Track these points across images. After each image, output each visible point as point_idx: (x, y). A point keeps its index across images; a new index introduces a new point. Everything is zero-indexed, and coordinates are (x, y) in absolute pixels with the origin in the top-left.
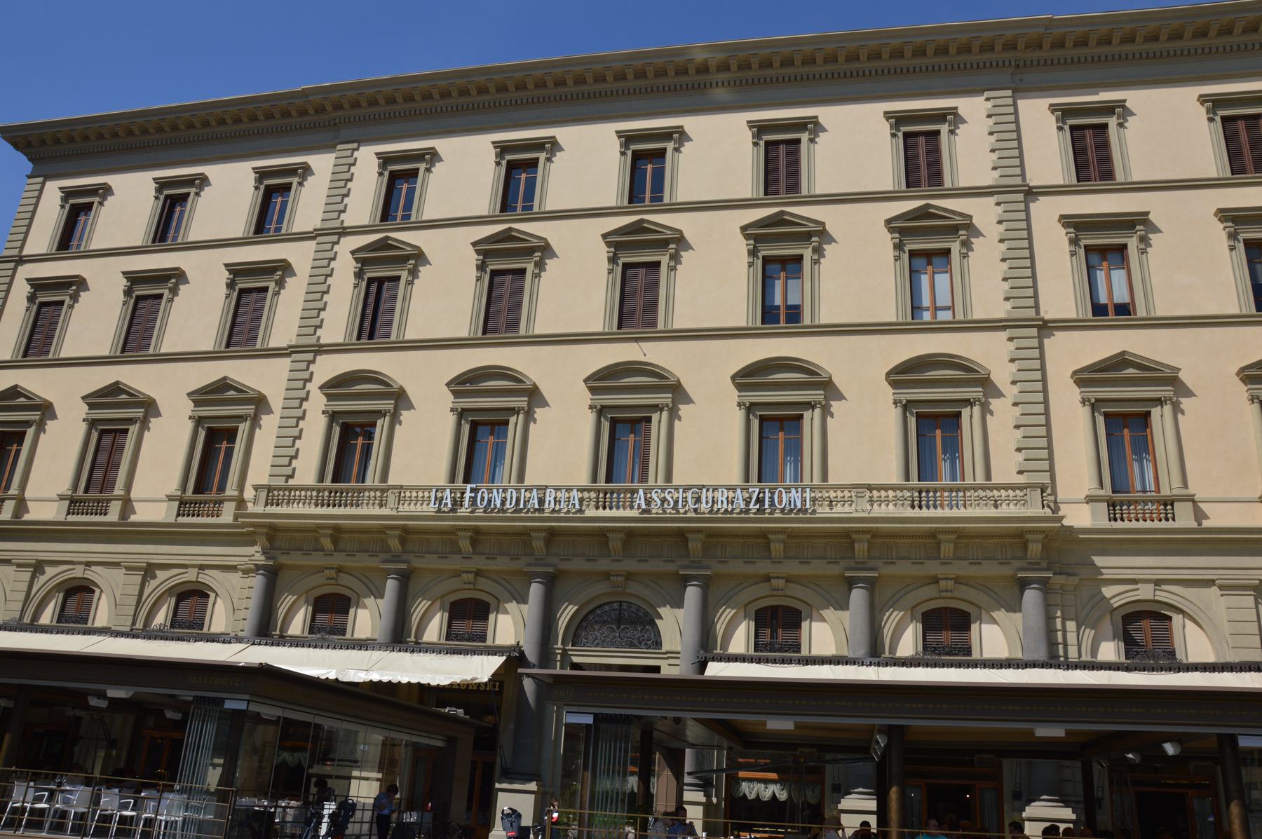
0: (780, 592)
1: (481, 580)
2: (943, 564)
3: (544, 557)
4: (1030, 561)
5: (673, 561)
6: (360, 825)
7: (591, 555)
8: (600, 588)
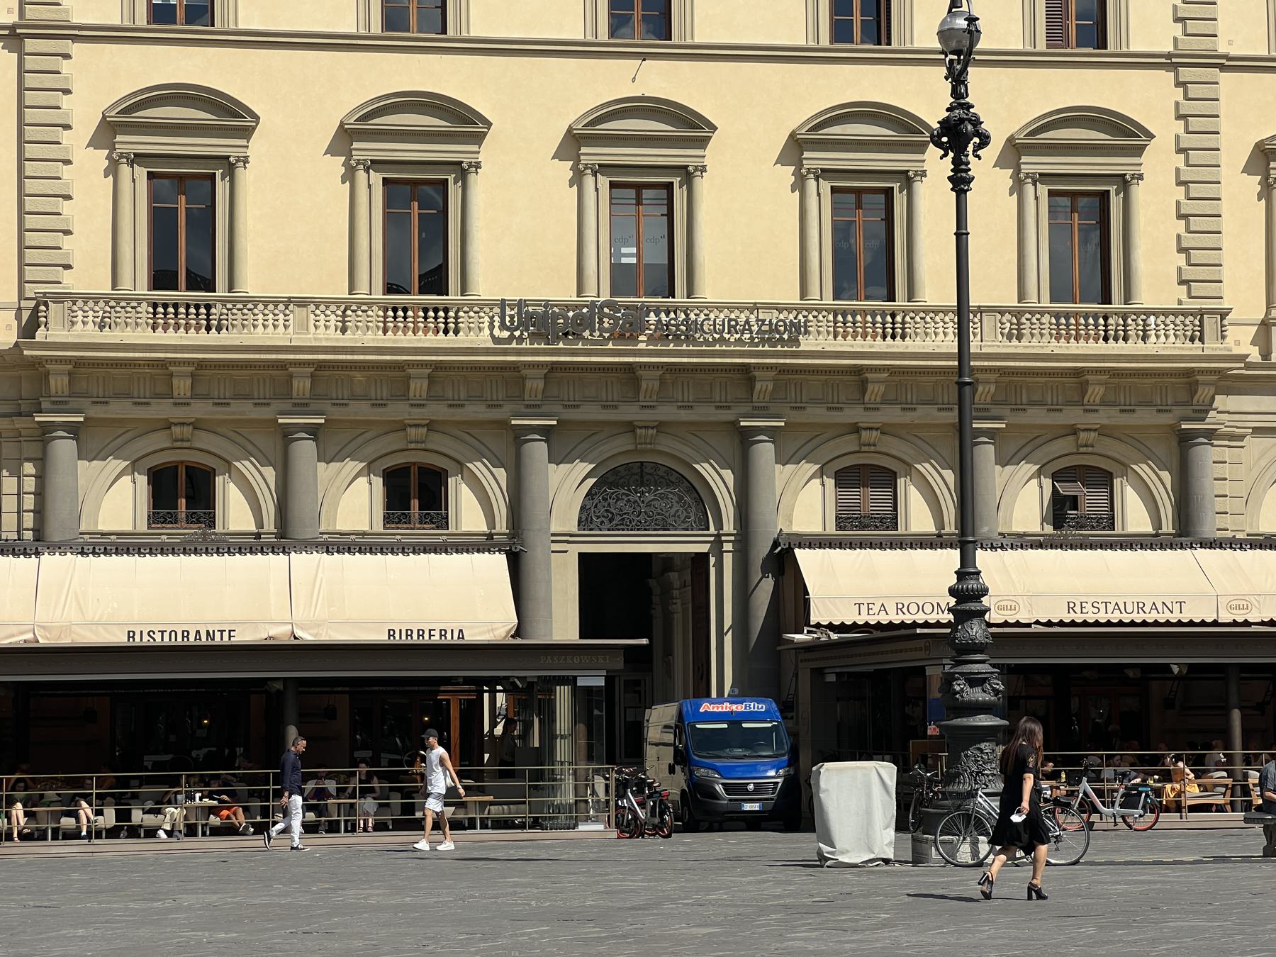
0: (419, 445)
1: (436, 437)
2: (1086, 411)
3: (539, 403)
4: (756, 405)
5: (729, 408)
6: (1274, 817)
7: (610, 398)
8: (622, 443)
